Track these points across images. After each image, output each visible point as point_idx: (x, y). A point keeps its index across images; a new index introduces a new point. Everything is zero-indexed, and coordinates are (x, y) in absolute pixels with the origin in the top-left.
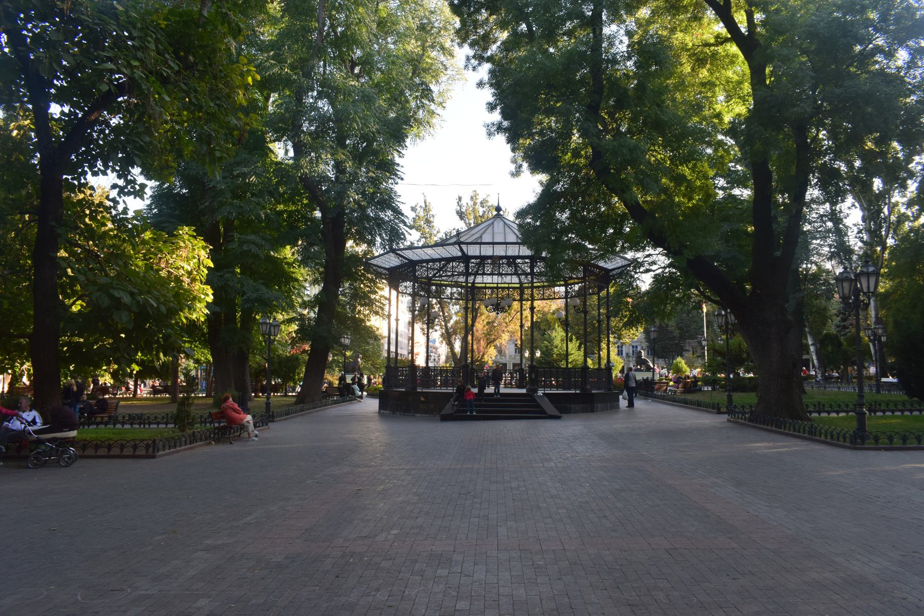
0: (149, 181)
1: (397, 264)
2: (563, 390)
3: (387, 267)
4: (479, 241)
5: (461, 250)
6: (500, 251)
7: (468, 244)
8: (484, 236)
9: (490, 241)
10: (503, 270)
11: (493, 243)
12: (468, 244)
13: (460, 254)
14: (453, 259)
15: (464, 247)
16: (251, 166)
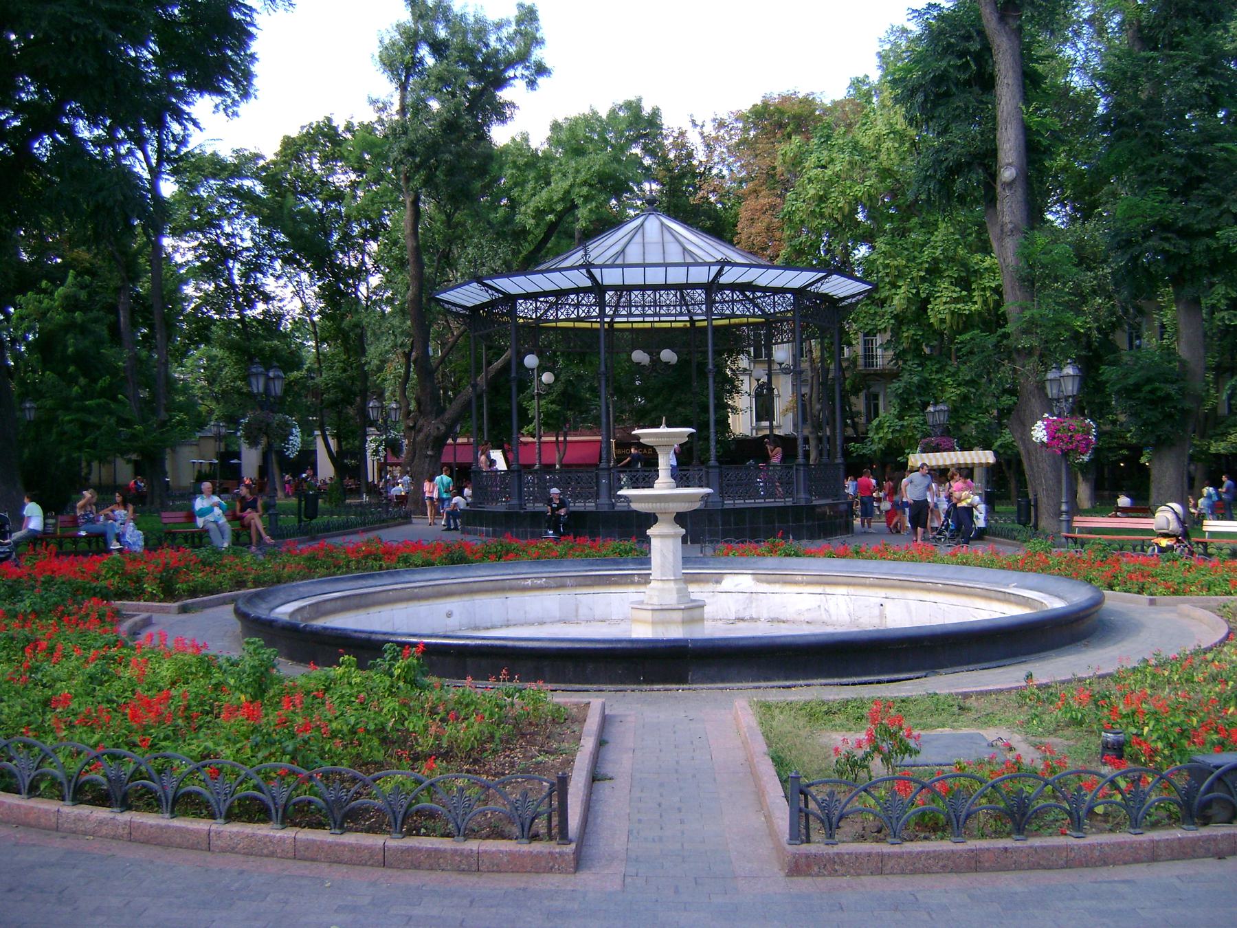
0: (1118, 344)
2: (598, 342)
3: (469, 305)
4: (619, 262)
5: (591, 277)
6: (655, 276)
7: (601, 267)
8: (628, 250)
9: (641, 261)
10: (676, 295)
11: (644, 266)
12: (601, 267)
13: (588, 283)
14: (578, 291)
15: (596, 272)
16: (419, 403)
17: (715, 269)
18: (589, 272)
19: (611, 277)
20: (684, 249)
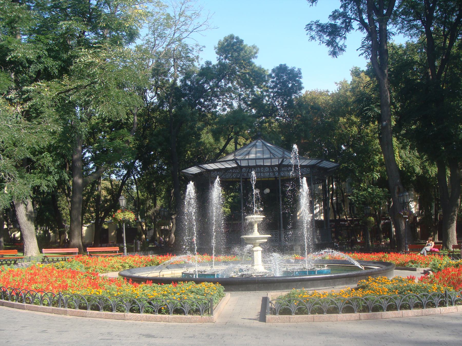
1: (199, 172)
7: (240, 160)
17: (281, 160)
18: (236, 162)
19: (244, 164)
20: (271, 153)
